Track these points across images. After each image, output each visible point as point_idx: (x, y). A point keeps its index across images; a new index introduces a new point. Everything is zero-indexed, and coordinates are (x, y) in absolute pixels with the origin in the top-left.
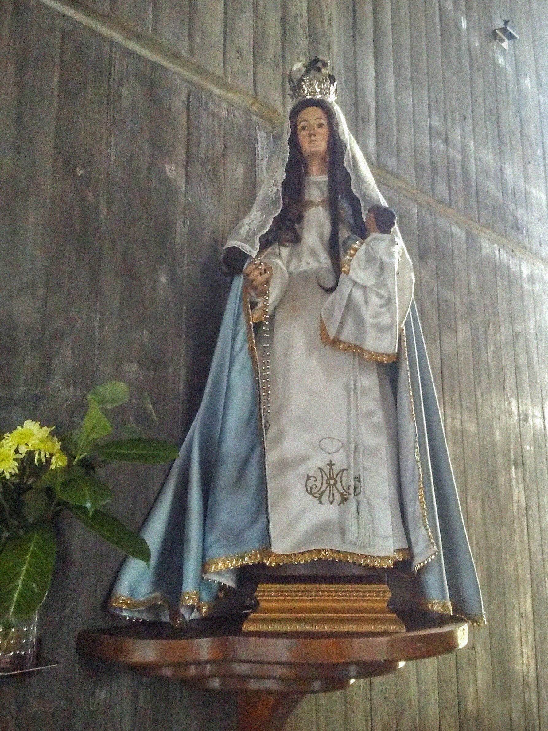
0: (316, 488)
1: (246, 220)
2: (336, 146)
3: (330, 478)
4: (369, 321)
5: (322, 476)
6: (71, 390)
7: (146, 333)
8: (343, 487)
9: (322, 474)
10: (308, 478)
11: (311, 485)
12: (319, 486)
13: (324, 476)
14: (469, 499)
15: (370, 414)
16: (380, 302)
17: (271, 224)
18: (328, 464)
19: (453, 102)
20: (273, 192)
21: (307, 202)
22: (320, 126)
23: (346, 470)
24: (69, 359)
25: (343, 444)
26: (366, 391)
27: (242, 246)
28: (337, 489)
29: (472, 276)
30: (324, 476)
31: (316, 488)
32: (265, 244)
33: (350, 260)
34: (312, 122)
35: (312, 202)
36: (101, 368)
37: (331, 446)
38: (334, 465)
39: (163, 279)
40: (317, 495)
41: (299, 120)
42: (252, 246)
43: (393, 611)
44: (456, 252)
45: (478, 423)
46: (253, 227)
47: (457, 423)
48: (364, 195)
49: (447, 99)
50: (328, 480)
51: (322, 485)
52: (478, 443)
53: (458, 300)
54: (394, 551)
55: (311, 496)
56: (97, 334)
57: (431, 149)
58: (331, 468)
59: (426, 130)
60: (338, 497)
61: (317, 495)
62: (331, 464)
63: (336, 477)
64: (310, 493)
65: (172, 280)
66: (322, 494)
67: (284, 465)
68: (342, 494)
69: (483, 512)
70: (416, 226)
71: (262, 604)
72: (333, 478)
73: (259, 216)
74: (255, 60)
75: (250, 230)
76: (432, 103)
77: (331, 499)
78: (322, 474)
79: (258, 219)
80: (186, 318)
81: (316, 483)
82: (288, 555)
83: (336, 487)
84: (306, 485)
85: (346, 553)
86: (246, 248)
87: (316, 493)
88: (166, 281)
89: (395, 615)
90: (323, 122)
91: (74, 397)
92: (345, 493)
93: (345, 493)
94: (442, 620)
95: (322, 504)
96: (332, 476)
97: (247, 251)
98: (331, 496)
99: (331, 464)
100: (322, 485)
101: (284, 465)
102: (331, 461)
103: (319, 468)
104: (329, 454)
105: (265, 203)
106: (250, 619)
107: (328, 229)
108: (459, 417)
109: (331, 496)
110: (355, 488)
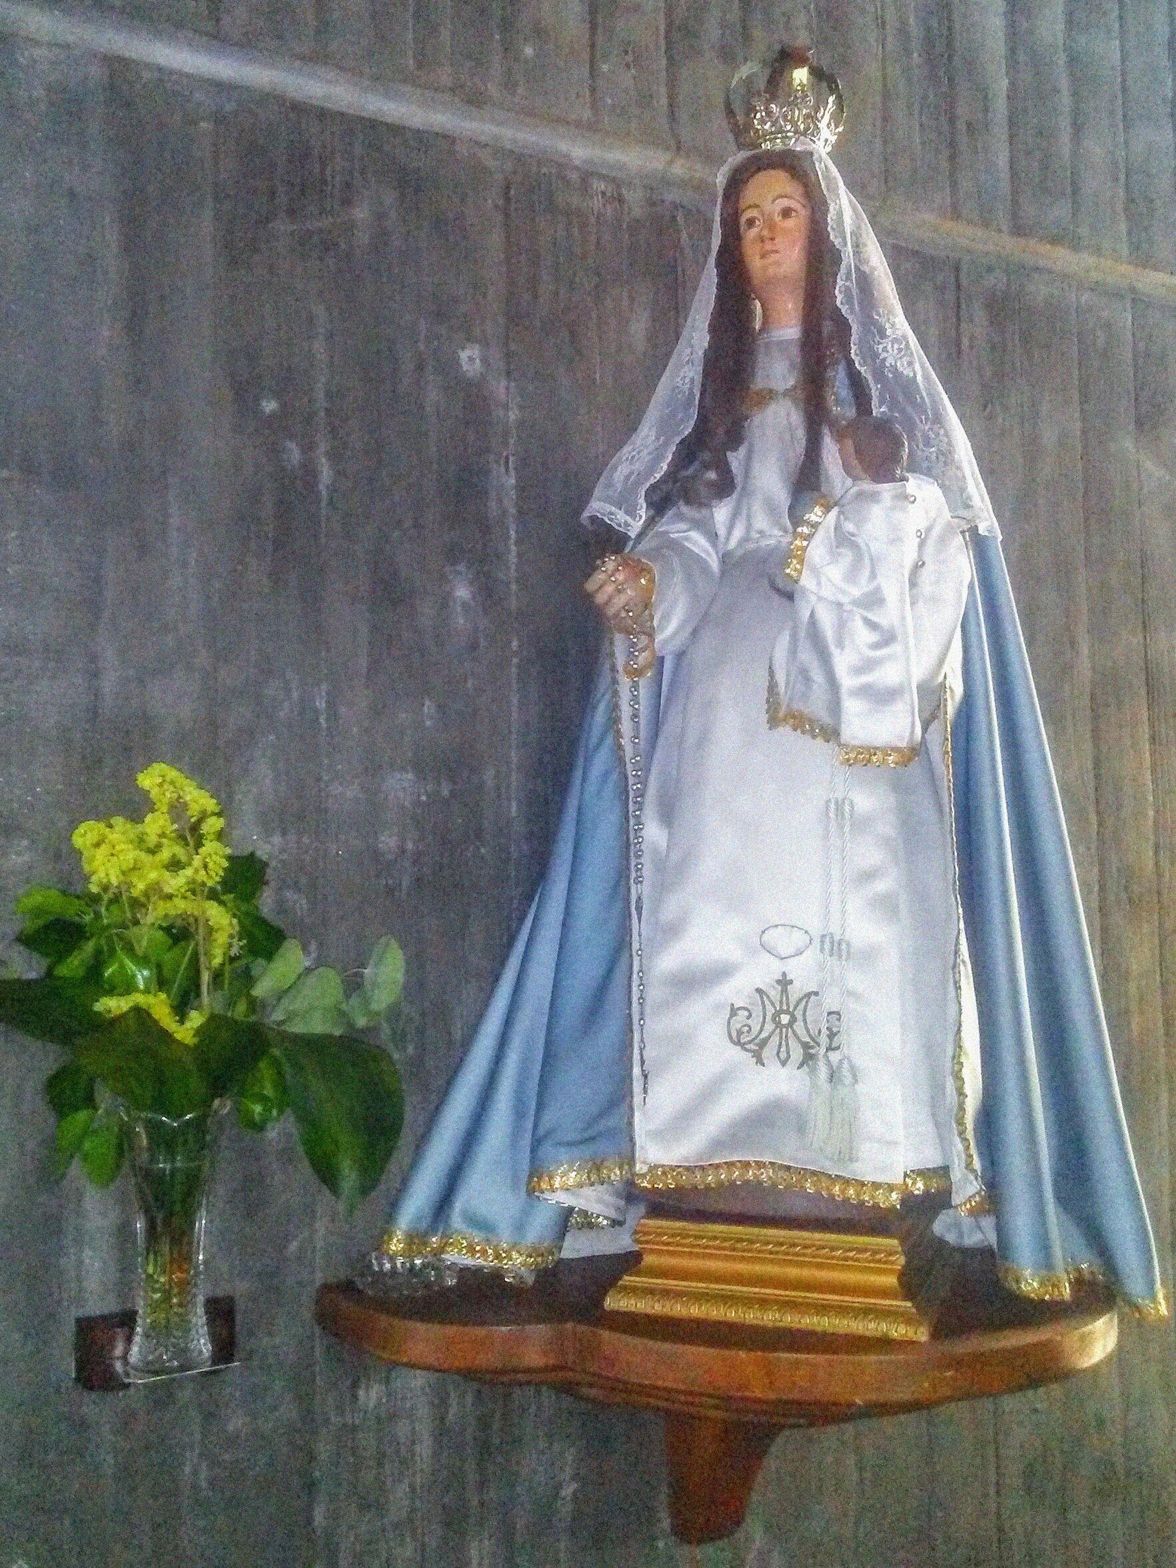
0: (749, 1032)
2: (820, 256)
3: (782, 1012)
4: (847, 682)
5: (764, 1007)
7: (429, 707)
8: (808, 1031)
9: (763, 1003)
10: (734, 1011)
11: (739, 1026)
12: (756, 1029)
15: (868, 876)
16: (870, 637)
18: (778, 982)
22: (786, 213)
23: (816, 994)
31: (749, 1032)
32: (660, 503)
33: (804, 549)
34: (768, 207)
35: (771, 391)
36: (336, 789)
37: (784, 941)
38: (791, 982)
39: (462, 592)
40: (752, 1046)
41: (743, 204)
43: (909, 1295)
46: (638, 466)
51: (763, 1026)
58: (784, 991)
60: (797, 1053)
61: (752, 1046)
62: (784, 982)
63: (795, 1008)
64: (738, 1043)
65: (488, 592)
66: (763, 1044)
67: (689, 983)
68: (806, 1046)
72: (787, 1012)
74: (670, 59)
75: (632, 473)
77: (783, 1056)
78: (763, 1003)
79: (646, 452)
81: (750, 1022)
82: (688, 1169)
83: (794, 1032)
84: (729, 1023)
85: (804, 1173)
86: (619, 518)
87: (750, 1042)
89: (909, 1304)
90: (793, 204)
92: (812, 1044)
93: (812, 1044)
95: (763, 1065)
99: (784, 982)
100: (763, 1026)
101: (689, 983)
102: (784, 974)
103: (759, 991)
109: (783, 1049)
110: (832, 1035)
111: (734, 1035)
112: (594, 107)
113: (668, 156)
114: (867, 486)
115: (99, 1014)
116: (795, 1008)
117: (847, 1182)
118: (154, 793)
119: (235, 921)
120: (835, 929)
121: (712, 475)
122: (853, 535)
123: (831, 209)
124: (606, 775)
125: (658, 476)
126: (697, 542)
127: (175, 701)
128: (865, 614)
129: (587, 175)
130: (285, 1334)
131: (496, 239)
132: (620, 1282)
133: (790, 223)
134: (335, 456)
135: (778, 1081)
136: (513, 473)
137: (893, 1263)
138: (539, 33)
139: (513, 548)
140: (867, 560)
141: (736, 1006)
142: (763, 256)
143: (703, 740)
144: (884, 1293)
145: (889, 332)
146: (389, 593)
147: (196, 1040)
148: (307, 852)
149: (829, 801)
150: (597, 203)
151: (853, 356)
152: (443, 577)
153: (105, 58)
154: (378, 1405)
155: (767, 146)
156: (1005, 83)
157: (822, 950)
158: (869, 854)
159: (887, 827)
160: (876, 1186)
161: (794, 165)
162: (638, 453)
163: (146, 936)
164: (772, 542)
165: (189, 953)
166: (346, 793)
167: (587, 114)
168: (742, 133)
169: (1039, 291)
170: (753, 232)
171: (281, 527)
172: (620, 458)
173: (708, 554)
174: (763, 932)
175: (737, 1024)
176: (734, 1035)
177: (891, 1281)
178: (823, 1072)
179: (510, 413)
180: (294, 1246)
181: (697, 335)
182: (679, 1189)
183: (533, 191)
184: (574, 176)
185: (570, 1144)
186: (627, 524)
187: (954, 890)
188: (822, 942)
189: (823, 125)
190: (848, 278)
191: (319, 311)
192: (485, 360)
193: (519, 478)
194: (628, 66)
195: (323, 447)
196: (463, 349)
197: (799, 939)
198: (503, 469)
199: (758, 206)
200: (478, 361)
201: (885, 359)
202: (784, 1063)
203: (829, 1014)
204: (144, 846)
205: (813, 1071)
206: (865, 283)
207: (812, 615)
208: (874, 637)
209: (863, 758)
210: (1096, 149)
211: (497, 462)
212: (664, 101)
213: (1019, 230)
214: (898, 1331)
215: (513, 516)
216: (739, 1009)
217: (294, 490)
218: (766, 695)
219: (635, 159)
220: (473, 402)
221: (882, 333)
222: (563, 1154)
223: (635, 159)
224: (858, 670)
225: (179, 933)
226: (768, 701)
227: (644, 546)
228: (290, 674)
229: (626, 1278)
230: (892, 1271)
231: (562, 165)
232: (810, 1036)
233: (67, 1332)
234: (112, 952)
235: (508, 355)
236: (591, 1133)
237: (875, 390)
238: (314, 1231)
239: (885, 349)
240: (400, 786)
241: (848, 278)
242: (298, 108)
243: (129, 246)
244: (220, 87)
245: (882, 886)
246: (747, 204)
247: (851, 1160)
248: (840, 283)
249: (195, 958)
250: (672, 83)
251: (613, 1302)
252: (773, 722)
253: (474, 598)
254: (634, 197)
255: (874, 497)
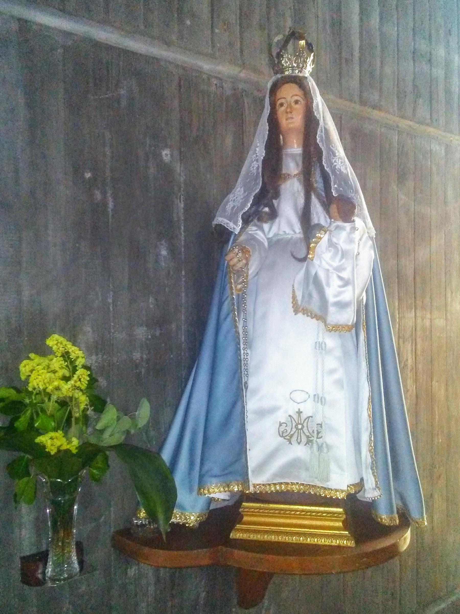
0: (286, 432)
1: (231, 196)
2: (310, 123)
4: (331, 299)
6: (94, 357)
7: (151, 300)
8: (309, 431)
9: (292, 421)
10: (281, 425)
11: (283, 430)
12: (289, 431)
13: (293, 422)
14: (434, 382)
15: (332, 371)
17: (251, 202)
18: (297, 412)
19: (439, 20)
20: (255, 168)
21: (284, 174)
22: (296, 102)
23: (312, 417)
24: (90, 334)
25: (309, 396)
26: (330, 352)
27: (227, 224)
28: (304, 432)
29: (449, 189)
30: (293, 422)
34: (289, 99)
35: (289, 175)
37: (298, 396)
38: (302, 412)
39: (164, 252)
42: (236, 223)
44: (434, 169)
45: (446, 319)
46: (237, 204)
47: (427, 323)
48: (334, 170)
49: (433, 18)
50: (297, 425)
52: (445, 336)
53: (434, 213)
54: (348, 486)
55: (282, 438)
56: (111, 309)
57: (414, 73)
58: (299, 416)
59: (410, 56)
60: (304, 439)
61: (288, 437)
62: (299, 413)
63: (304, 423)
65: (173, 251)
66: (292, 436)
67: (262, 413)
68: (308, 437)
69: (447, 390)
70: (396, 152)
71: (245, 519)
72: (301, 424)
73: (243, 192)
75: (234, 207)
76: (417, 25)
77: (299, 441)
78: (292, 421)
79: (240, 197)
80: (185, 281)
81: (286, 428)
82: (263, 485)
84: (279, 429)
86: (231, 226)
87: (286, 436)
88: (167, 254)
89: (347, 533)
91: (96, 362)
93: (310, 436)
94: (387, 531)
95: (291, 444)
96: (300, 422)
97: (231, 228)
98: (299, 438)
99: (299, 413)
101: (262, 413)
102: (299, 409)
104: (298, 403)
105: (247, 179)
106: (236, 529)
107: (301, 201)
108: (428, 316)
109: (299, 438)
110: (318, 433)
111: (281, 433)
112: (213, 47)
113: (239, 69)
114: (340, 223)
115: (37, 444)
116: (304, 423)
117: (325, 489)
118: (55, 348)
119: (87, 398)
120: (320, 392)
121: (267, 209)
122: (336, 244)
123: (314, 101)
124: (228, 332)
125: (246, 209)
126: (260, 235)
127: (53, 303)
128: (337, 273)
129: (210, 77)
130: (100, 554)
131: (176, 103)
132: (236, 528)
133: (297, 106)
134: (115, 198)
135: (299, 451)
136: (182, 202)
137: (340, 517)
138: (193, 16)
139: (183, 233)
140: (340, 252)
141: (282, 422)
142: (287, 120)
143: (264, 316)
144: (338, 529)
145: (337, 154)
146: (137, 254)
147: (77, 451)
148: (106, 362)
149: (316, 343)
150: (213, 88)
151: (323, 163)
152: (156, 246)
153: (19, 20)
154: (135, 574)
155: (287, 73)
156: (358, 43)
157: (314, 401)
158: (332, 362)
159: (338, 353)
160: (337, 490)
161: (299, 82)
162: (237, 198)
163: (51, 406)
164: (289, 236)
165: (68, 411)
166: (121, 336)
167: (210, 51)
168: (276, 67)
169: (368, 127)
170: (283, 108)
171: (93, 228)
172: (229, 199)
173: (264, 240)
174: (291, 393)
175: (282, 429)
176: (281, 433)
177: (340, 524)
178: (315, 446)
179: (181, 178)
180: (103, 519)
181: (258, 150)
182: (261, 493)
183: (189, 82)
184: (205, 76)
185: (215, 476)
186: (234, 229)
187: (368, 379)
188: (314, 398)
189: (308, 65)
190: (322, 132)
191: (108, 135)
192: (172, 156)
193: (186, 205)
194: (225, 30)
195: (109, 195)
196: (163, 150)
197: (305, 396)
198: (179, 201)
199: (284, 98)
200: (169, 156)
201: (336, 165)
202: (299, 443)
203: (317, 424)
204: (50, 370)
205: (311, 447)
206: (327, 132)
207: (316, 274)
208: (340, 283)
209: (336, 328)
210: (388, 70)
211: (177, 198)
212: (239, 45)
213: (363, 102)
214: (345, 543)
215: (183, 220)
216: (283, 423)
217: (98, 209)
218: (291, 300)
219: (226, 69)
220: (166, 171)
221: (334, 155)
222: (214, 480)
223: (226, 69)
224: (336, 296)
225: (64, 403)
226: (292, 303)
227: (242, 238)
228: (98, 289)
229: (238, 526)
230: (340, 521)
231: (200, 71)
232: (309, 433)
233: (18, 563)
234: (38, 415)
235: (181, 152)
236: (226, 472)
237: (332, 178)
238: (110, 511)
239: (335, 162)
240: (141, 332)
241: (322, 132)
242: (97, 45)
243: (30, 106)
244: (67, 34)
245: (337, 376)
246: (279, 97)
247: (327, 481)
248: (318, 133)
249: (70, 413)
250: (242, 38)
251: (234, 535)
252: (296, 311)
253: (168, 254)
254: (227, 86)
255: (343, 228)
